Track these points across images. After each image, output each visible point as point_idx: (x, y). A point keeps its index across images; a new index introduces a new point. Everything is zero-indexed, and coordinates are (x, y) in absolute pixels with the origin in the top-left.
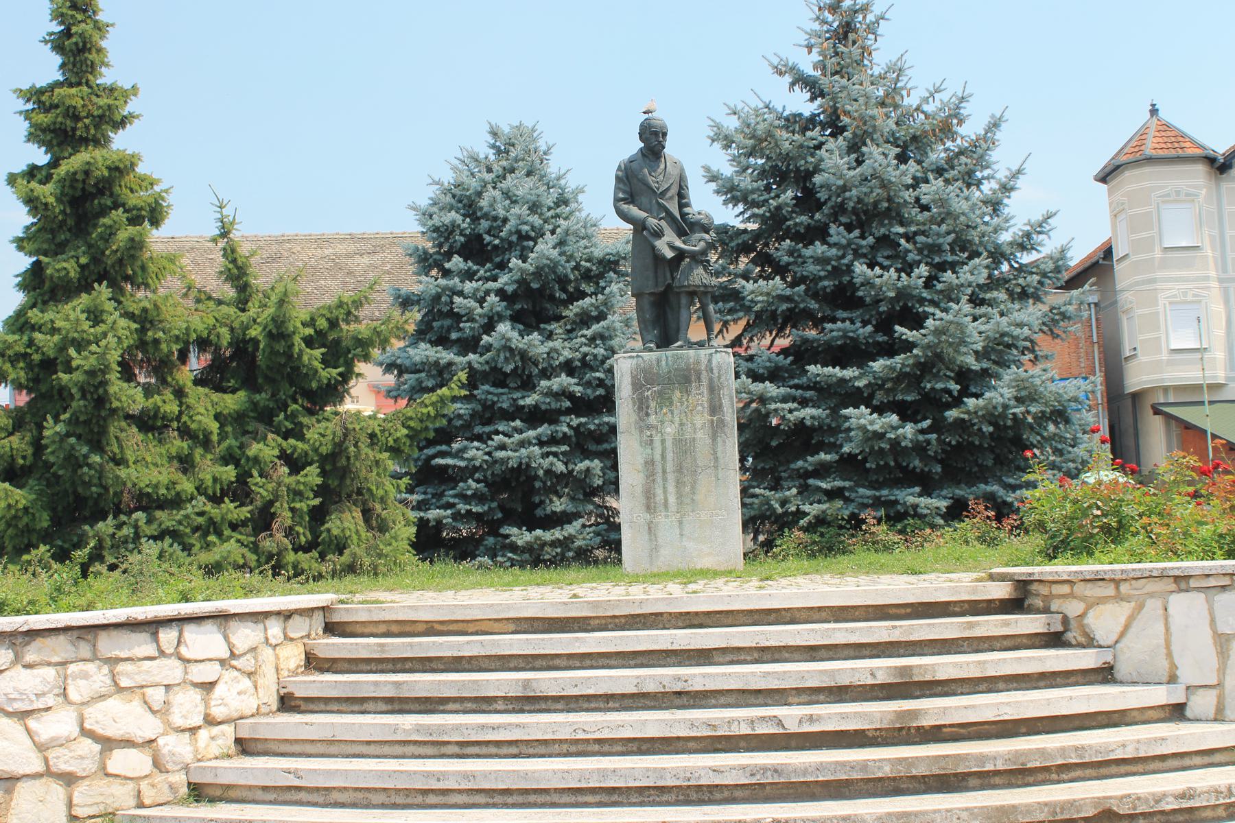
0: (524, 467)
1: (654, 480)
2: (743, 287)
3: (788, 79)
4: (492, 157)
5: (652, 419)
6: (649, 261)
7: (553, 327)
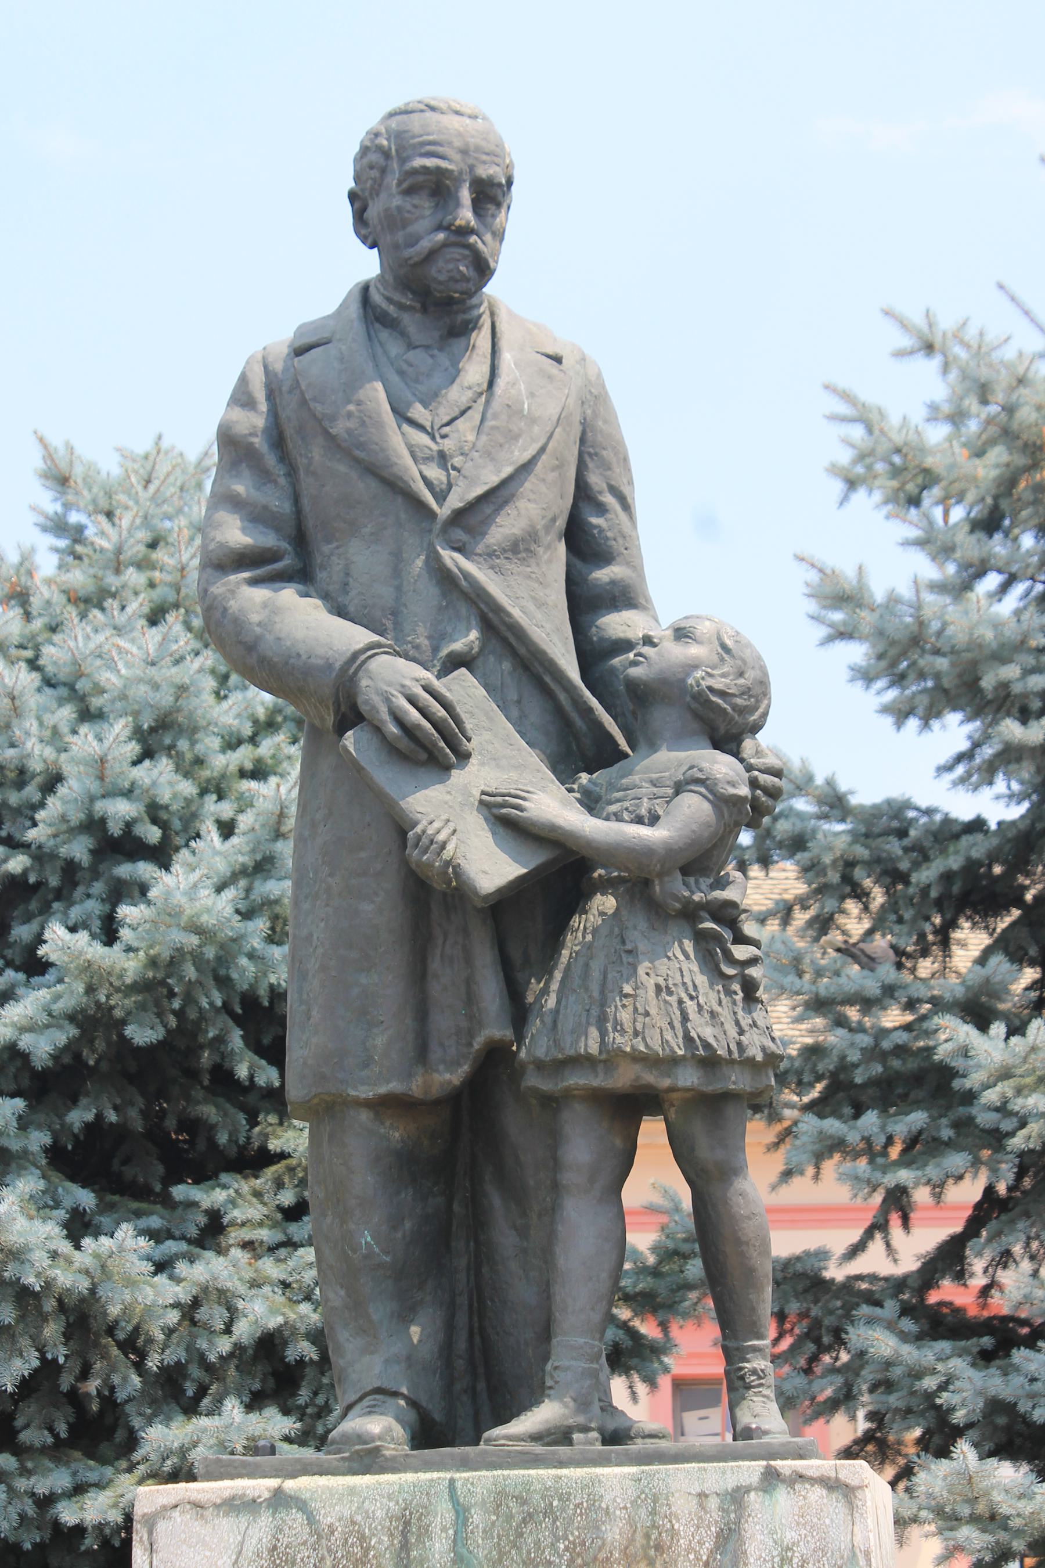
2: (965, 1052)
4: (47, 564)
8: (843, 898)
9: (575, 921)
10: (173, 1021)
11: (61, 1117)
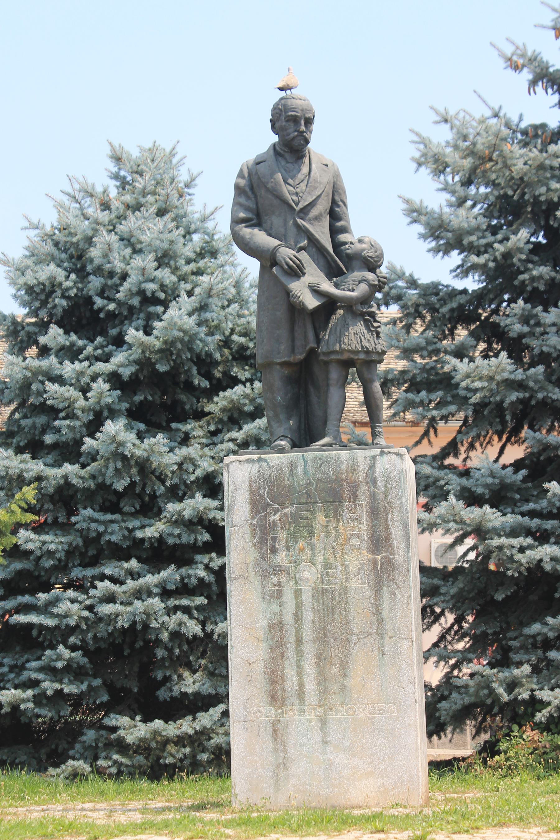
0: (139, 627)
1: (283, 654)
2: (455, 370)
3: (526, 75)
4: (113, 193)
5: (282, 558)
6: (282, 313)
7: (188, 427)
8: (415, 319)
9: (333, 317)
10: (172, 363)
11: (132, 398)
